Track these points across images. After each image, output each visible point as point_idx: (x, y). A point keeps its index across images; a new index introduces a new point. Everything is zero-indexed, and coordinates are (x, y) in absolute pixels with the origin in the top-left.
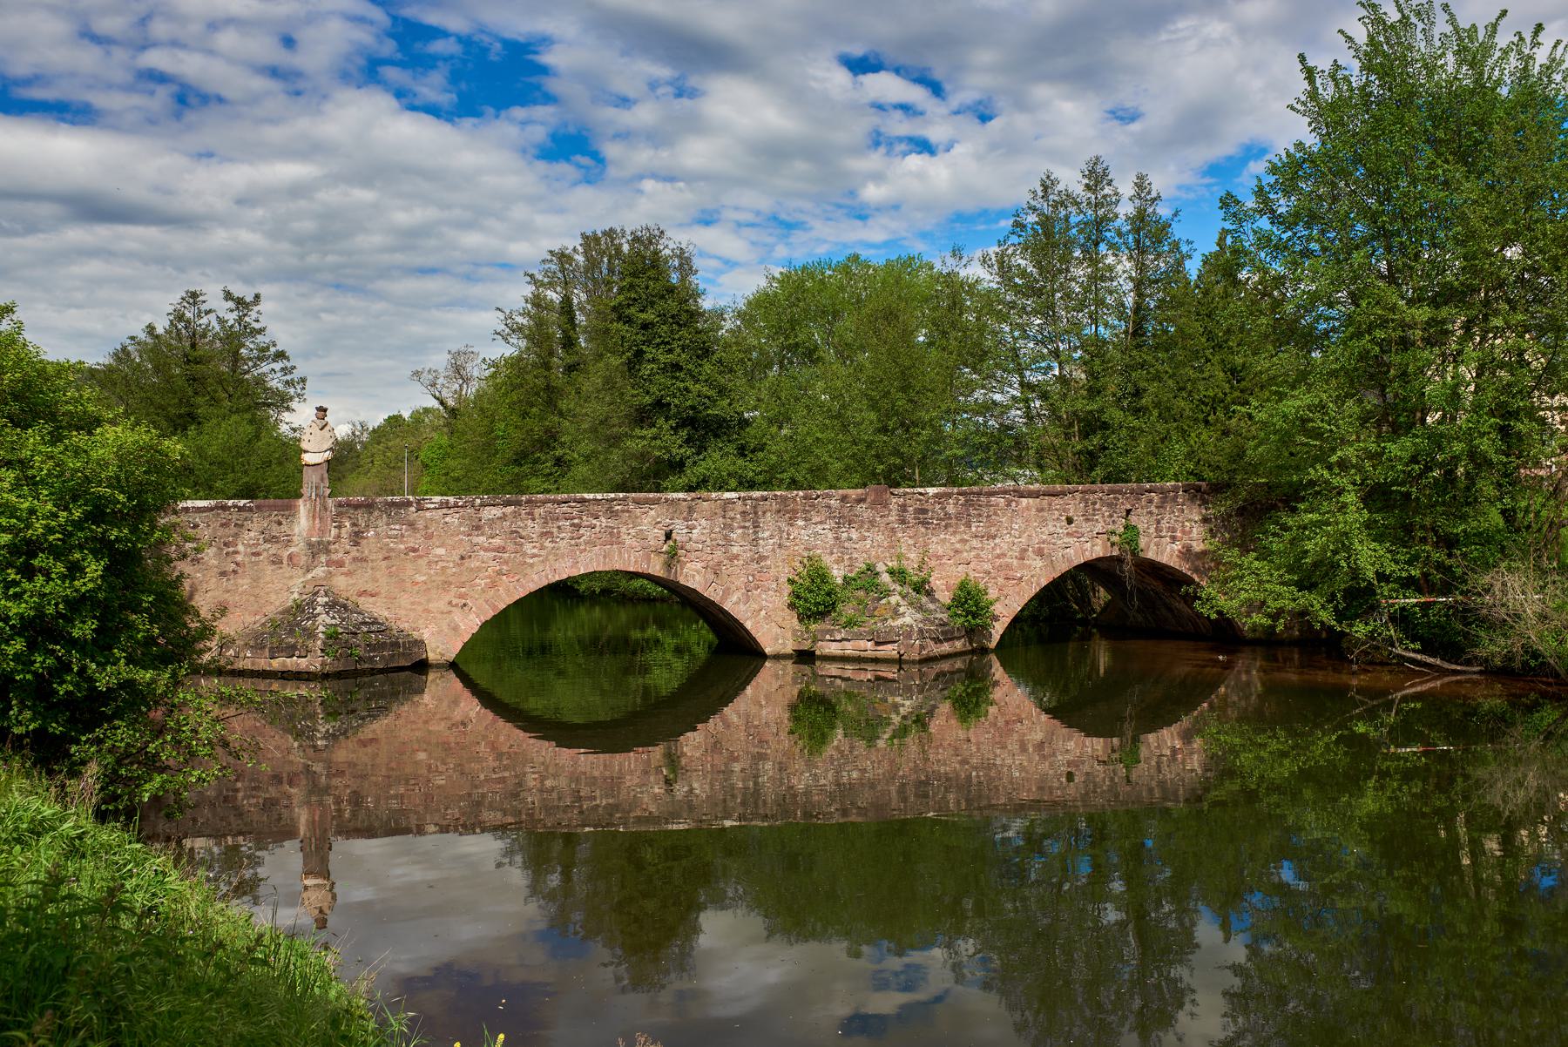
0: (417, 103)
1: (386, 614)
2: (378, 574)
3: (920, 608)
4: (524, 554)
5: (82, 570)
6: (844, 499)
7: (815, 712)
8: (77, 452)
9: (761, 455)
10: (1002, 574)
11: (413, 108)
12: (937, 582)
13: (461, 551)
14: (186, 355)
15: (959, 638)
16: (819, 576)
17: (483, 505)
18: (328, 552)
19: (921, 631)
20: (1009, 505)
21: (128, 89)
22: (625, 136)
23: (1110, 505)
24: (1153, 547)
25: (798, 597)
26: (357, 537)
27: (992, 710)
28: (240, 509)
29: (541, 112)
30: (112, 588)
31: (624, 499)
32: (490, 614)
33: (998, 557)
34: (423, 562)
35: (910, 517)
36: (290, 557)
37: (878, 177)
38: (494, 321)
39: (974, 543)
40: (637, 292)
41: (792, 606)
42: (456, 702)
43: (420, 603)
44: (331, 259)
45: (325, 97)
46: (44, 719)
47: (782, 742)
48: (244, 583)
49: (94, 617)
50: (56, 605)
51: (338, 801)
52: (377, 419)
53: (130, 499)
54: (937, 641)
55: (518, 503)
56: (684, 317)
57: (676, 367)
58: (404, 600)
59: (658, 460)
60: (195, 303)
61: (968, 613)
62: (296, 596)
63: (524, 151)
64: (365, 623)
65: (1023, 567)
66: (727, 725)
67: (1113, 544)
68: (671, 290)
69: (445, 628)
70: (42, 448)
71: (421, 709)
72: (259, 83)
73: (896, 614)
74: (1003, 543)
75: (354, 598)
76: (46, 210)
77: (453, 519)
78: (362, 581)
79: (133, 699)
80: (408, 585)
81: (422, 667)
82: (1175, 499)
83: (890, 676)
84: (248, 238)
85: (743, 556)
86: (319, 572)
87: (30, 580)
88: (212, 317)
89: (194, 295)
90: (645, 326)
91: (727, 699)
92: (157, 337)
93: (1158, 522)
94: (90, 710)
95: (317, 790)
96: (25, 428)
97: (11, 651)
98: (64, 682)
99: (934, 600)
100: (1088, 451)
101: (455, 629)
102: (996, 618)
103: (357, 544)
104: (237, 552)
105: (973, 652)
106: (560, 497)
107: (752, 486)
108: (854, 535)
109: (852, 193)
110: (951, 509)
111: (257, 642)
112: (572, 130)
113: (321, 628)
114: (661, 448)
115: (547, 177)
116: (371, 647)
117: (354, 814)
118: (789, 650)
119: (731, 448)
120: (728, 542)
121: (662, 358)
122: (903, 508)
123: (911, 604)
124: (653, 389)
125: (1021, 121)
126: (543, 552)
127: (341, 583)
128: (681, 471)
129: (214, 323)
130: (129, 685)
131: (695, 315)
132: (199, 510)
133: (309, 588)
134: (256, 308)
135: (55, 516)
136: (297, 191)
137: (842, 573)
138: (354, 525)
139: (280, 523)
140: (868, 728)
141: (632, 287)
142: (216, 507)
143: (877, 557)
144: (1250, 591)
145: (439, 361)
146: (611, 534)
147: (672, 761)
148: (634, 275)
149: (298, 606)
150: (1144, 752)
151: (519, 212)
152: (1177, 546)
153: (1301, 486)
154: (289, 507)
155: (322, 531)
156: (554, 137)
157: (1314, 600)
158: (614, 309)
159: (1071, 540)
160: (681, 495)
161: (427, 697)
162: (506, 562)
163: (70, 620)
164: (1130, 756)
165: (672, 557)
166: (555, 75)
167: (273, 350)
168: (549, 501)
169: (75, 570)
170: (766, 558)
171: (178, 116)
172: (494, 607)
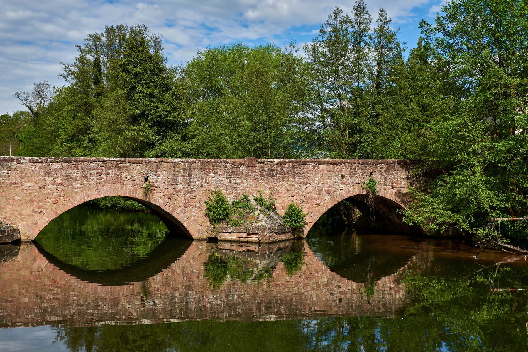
3: (270, 218)
4: (73, 187)
6: (233, 163)
7: (217, 267)
9: (193, 140)
10: (310, 202)
12: (278, 205)
13: (40, 185)
15: (288, 233)
16: (221, 201)
17: (52, 162)
20: (314, 168)
23: (362, 170)
25: (210, 211)
27: (304, 267)
31: (124, 161)
32: (54, 217)
33: (308, 193)
34: (19, 190)
35: (265, 173)
38: (59, 69)
39: (297, 186)
41: (207, 215)
42: (35, 260)
43: (17, 211)
47: (199, 281)
54: (278, 234)
55: (70, 161)
56: (156, 71)
57: (152, 96)
59: (142, 142)
65: (319, 198)
66: (173, 272)
67: (363, 189)
68: (150, 57)
69: (30, 223)
73: (258, 220)
74: (311, 187)
77: (36, 169)
80: (11, 201)
81: (18, 242)
83: (254, 249)
85: (184, 191)
90: (137, 75)
93: (385, 178)
99: (276, 214)
100: (350, 143)
101: (36, 224)
102: (306, 223)
105: (295, 239)
106: (91, 159)
107: (189, 155)
108: (238, 181)
109: (241, 14)
110: (285, 169)
118: (205, 237)
122: (262, 168)
123: (265, 215)
124: (140, 106)
126: (82, 186)
128: (153, 148)
131: (161, 70)
137: (232, 199)
140: (242, 275)
141: (130, 55)
143: (249, 192)
146: (117, 178)
147: (146, 291)
148: (131, 49)
152: (394, 190)
159: (343, 186)
162: (63, 191)
164: (370, 291)
165: (148, 190)
168: (86, 161)
170: (195, 191)
172: (56, 213)
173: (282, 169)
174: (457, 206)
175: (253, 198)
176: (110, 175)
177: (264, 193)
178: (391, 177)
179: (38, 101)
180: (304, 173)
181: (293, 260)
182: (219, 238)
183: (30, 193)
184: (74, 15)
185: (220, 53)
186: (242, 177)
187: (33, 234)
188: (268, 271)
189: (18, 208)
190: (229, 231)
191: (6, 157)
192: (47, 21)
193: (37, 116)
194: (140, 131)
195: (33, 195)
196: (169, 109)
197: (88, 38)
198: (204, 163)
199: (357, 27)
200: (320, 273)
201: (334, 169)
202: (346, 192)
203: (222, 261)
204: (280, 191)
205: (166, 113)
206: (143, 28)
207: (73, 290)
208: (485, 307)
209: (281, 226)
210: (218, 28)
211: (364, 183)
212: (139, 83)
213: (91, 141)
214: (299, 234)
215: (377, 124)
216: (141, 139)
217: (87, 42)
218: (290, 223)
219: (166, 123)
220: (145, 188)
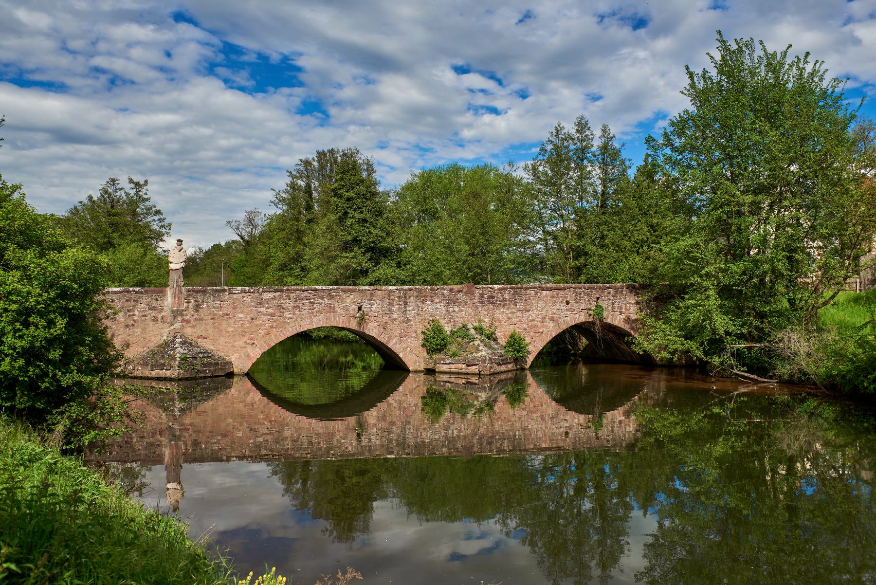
0: (234, 85)
1: (212, 348)
2: (208, 327)
3: (490, 347)
4: (285, 317)
5: (55, 324)
6: (451, 290)
7: (435, 400)
8: (53, 262)
9: (409, 267)
11: (232, 88)
12: (499, 334)
13: (252, 315)
14: (108, 212)
18: (182, 315)
19: (490, 359)
20: (536, 294)
21: (85, 76)
22: (338, 104)
23: (588, 295)
24: (610, 316)
25: (427, 341)
26: (197, 308)
28: (136, 292)
29: (297, 91)
30: (70, 333)
31: (337, 289)
32: (267, 348)
33: (531, 321)
34: (232, 321)
35: (485, 300)
36: (162, 318)
37: (469, 126)
38: (270, 196)
39: (519, 314)
40: (341, 181)
41: (423, 346)
42: (248, 393)
44: (186, 163)
45: (187, 81)
46: (34, 401)
48: (138, 331)
50: (41, 341)
52: (207, 246)
53: (80, 287)
54: (499, 364)
55: (282, 291)
56: (369, 195)
57: (365, 221)
58: (222, 341)
59: (355, 270)
60: (113, 185)
62: (165, 338)
63: (289, 110)
64: (201, 353)
65: (543, 326)
66: (389, 405)
68: (362, 181)
69: (243, 355)
72: (153, 74)
74: (533, 314)
75: (195, 339)
76: (40, 136)
77: (248, 299)
78: (200, 330)
79: (80, 391)
80: (224, 333)
81: (231, 375)
85: (399, 320)
86: (177, 325)
88: (122, 192)
89: (113, 180)
90: (349, 199)
92: (94, 202)
93: (613, 304)
94: (59, 397)
96: (26, 249)
97: (17, 365)
99: (497, 343)
100: (576, 266)
102: (529, 353)
103: (197, 311)
105: (517, 370)
106: (303, 288)
107: (404, 283)
108: (456, 309)
109: (456, 134)
110: (506, 296)
112: (313, 100)
113: (178, 355)
118: (422, 368)
119: (393, 264)
121: (357, 216)
122: (482, 295)
123: (485, 345)
124: (353, 232)
125: (543, 98)
126: (295, 317)
127: (188, 331)
129: (123, 195)
130: (78, 384)
131: (374, 194)
132: (115, 293)
133: (172, 334)
136: (170, 128)
137: (450, 329)
138: (196, 301)
139: (157, 300)
141: (342, 179)
142: (124, 291)
145: (241, 216)
146: (330, 307)
147: (361, 425)
148: (343, 173)
149: (166, 343)
150: (605, 421)
151: (285, 141)
152: (623, 317)
155: (179, 305)
156: (304, 103)
162: (275, 321)
163: (48, 350)
164: (598, 425)
165: (362, 320)
167: (154, 209)
168: (298, 290)
169: (51, 324)
170: (410, 320)
171: (109, 90)
172: (269, 345)
184: (285, 141)
187: (246, 366)
188: (490, 405)
189: (231, 340)
191: (218, 288)
192: (258, 147)
196: (383, 234)
198: (420, 290)
204: (501, 318)
211: (590, 309)
213: (303, 269)
215: (602, 247)
218: (511, 354)
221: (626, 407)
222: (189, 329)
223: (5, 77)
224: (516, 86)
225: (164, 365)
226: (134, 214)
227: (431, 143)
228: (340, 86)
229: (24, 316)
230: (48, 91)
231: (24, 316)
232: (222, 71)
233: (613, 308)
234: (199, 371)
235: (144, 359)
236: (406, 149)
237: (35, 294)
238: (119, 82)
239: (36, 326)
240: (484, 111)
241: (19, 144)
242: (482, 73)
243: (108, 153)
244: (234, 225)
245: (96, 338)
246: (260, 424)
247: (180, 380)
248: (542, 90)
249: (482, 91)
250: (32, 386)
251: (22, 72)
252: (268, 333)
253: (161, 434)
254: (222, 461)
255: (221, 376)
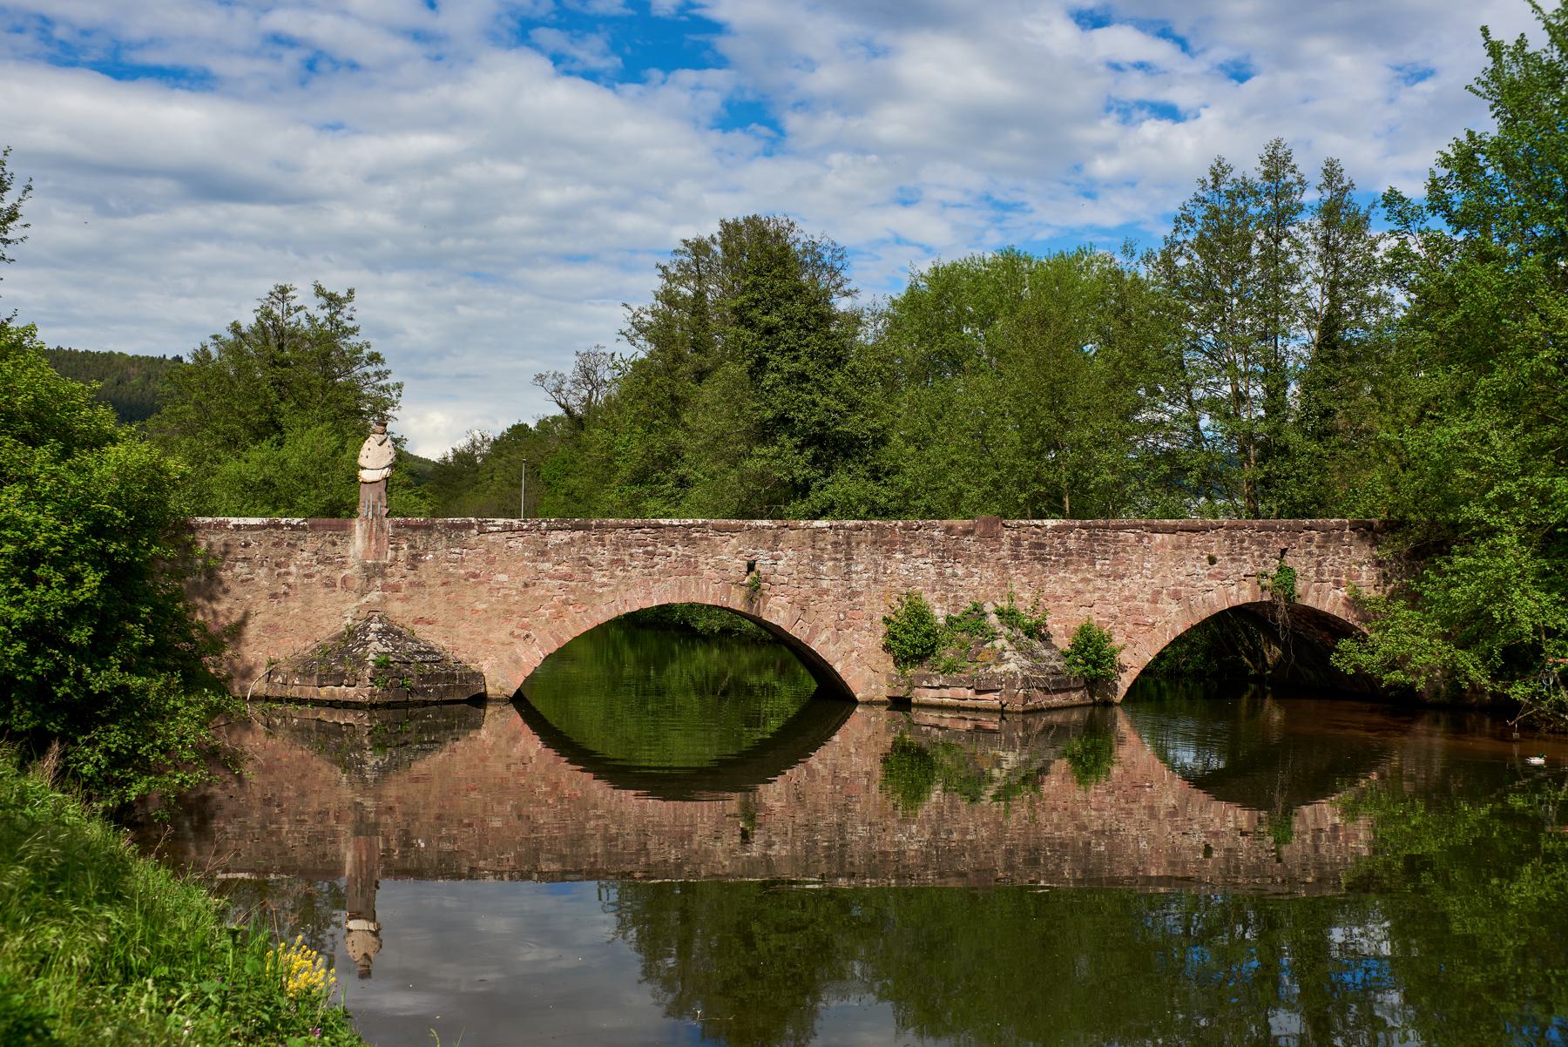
0: (575, 67)
1: (443, 643)
2: (436, 601)
3: (1031, 654)
4: (593, 583)
5: (81, 581)
6: (949, 530)
7: (910, 765)
8: (80, 470)
9: (896, 479)
10: (1131, 618)
11: (569, 73)
12: (1054, 626)
13: (525, 578)
14: (272, 357)
15: (1076, 690)
16: (919, 615)
17: (549, 529)
18: (384, 575)
19: (1026, 679)
20: (1140, 540)
21: (251, 54)
22: (804, 105)
23: (1260, 543)
24: (1312, 592)
25: (894, 638)
26: (414, 561)
27: (1116, 771)
28: (294, 528)
29: (713, 76)
30: (109, 598)
31: (703, 525)
32: (554, 647)
33: (1127, 599)
34: (483, 589)
35: (1024, 551)
36: (344, 580)
37: (1109, 149)
38: (621, 318)
39: (1099, 583)
40: (759, 291)
41: (887, 648)
42: (515, 739)
43: (479, 633)
44: (467, 243)
45: (471, 61)
46: (44, 719)
47: (871, 797)
48: (295, 606)
49: (92, 625)
50: (55, 611)
51: (387, 840)
52: (498, 427)
53: (129, 515)
54: (1047, 691)
55: (587, 528)
56: (813, 321)
57: (803, 377)
58: (463, 629)
59: (780, 482)
60: (284, 299)
61: (1088, 661)
62: (349, 621)
63: (696, 122)
64: (419, 652)
65: (1155, 611)
66: (812, 773)
67: (1264, 588)
68: (799, 290)
69: (506, 661)
70: (47, 467)
71: (477, 745)
72: (398, 47)
73: (1000, 659)
74: (1133, 584)
75: (410, 625)
76: (157, 186)
77: (517, 544)
78: (418, 608)
79: (125, 706)
80: (468, 613)
81: (480, 700)
82: (1339, 538)
83: (991, 726)
84: (379, 219)
85: (835, 594)
86: (374, 596)
87: (32, 588)
88: (302, 314)
89: (284, 290)
90: (769, 331)
91: (815, 745)
92: (243, 336)
93: (1319, 564)
94: (85, 713)
95: (365, 828)
96: (35, 446)
97: (12, 653)
98: (62, 685)
99: (1050, 646)
100: (1274, 479)
101: (517, 661)
102: (1123, 669)
103: (414, 568)
104: (288, 574)
105: (1094, 704)
106: (632, 522)
107: (886, 513)
108: (960, 571)
109: (1078, 168)
110: (1072, 544)
111: (305, 669)
112: (749, 96)
113: (372, 656)
114: (780, 468)
115: (720, 150)
116: (425, 678)
117: (403, 856)
118: (883, 696)
119: (861, 470)
120: (817, 575)
121: (786, 367)
122: (1017, 542)
123: (1019, 649)
124: (777, 402)
125: (1287, 80)
126: (613, 581)
127: (396, 608)
128: (805, 495)
129: (304, 322)
130: (123, 690)
131: (825, 319)
132: (251, 528)
133: (363, 614)
134: (349, 305)
135: (57, 529)
136: (433, 166)
137: (945, 612)
138: (412, 547)
139: (334, 544)
140: (971, 785)
141: (755, 286)
142: (269, 525)
143: (986, 596)
144: (1411, 647)
145: (569, 368)
146: (688, 563)
147: (750, 814)
148: (758, 273)
149: (351, 632)
150: (1297, 826)
151: (685, 190)
152: (1342, 593)
153: (1454, 526)
154: (344, 527)
155: (379, 553)
156: (729, 105)
157: (1466, 659)
158: (735, 311)
159: (1214, 583)
160: (766, 523)
161: (483, 732)
162: (573, 591)
163: (69, 628)
164: (1283, 833)
165: (754, 592)
166: (729, 32)
167: (366, 351)
168: (621, 526)
169: (74, 580)
170: (859, 594)
171: (303, 83)
172: (559, 640)
173: (1063, 544)
174: (1471, 628)
175: (993, 608)
176: (673, 558)
177: (1021, 599)
178: (1332, 561)
179: (585, 393)
180: (1116, 553)
181: (1091, 750)
182: (914, 700)
183: (505, 596)
184: (685, 190)
185: (969, 275)
186: (968, 562)
187: (513, 683)
188: (1033, 778)
189: (483, 629)
190: (936, 684)
191: (458, 520)
192: (623, 206)
193: (576, 423)
194: (773, 458)
195: (511, 600)
196: (842, 407)
197: (682, 247)
198: (881, 529)
199: (1269, 203)
200: (1156, 786)
201: (1189, 542)
202: (1220, 597)
203: (921, 753)
204: (1059, 593)
205: (836, 416)
206: (785, 225)
207: (595, 806)
208: (1528, 869)
209: (1058, 673)
210: (1023, 204)
211: (1264, 575)
212: (773, 348)
213: (682, 482)
214: (1104, 694)
215: (1320, 436)
216: (778, 475)
217: (679, 258)
218: (1080, 669)
219: (835, 440)
220: (748, 585)
221: (1347, 795)
222: (398, 603)
223: (83, 58)
224: (1221, 54)
225: (342, 675)
226: (325, 360)
227: (1019, 190)
228: (810, 64)
229: (28, 563)
230: (173, 87)
231: (28, 563)
232: (550, 37)
233: (1317, 573)
234: (413, 690)
235: (306, 662)
236: (961, 206)
237: (45, 526)
238: (323, 66)
239: (47, 582)
240: (1144, 113)
241: (113, 204)
242: (1142, 25)
243: (299, 222)
244: (551, 382)
245: (159, 610)
246: (538, 803)
247: (374, 706)
248: (1285, 60)
249: (1140, 66)
250: (40, 692)
251: (118, 47)
252: (559, 616)
253: (337, 818)
254: (460, 876)
255: (464, 701)
